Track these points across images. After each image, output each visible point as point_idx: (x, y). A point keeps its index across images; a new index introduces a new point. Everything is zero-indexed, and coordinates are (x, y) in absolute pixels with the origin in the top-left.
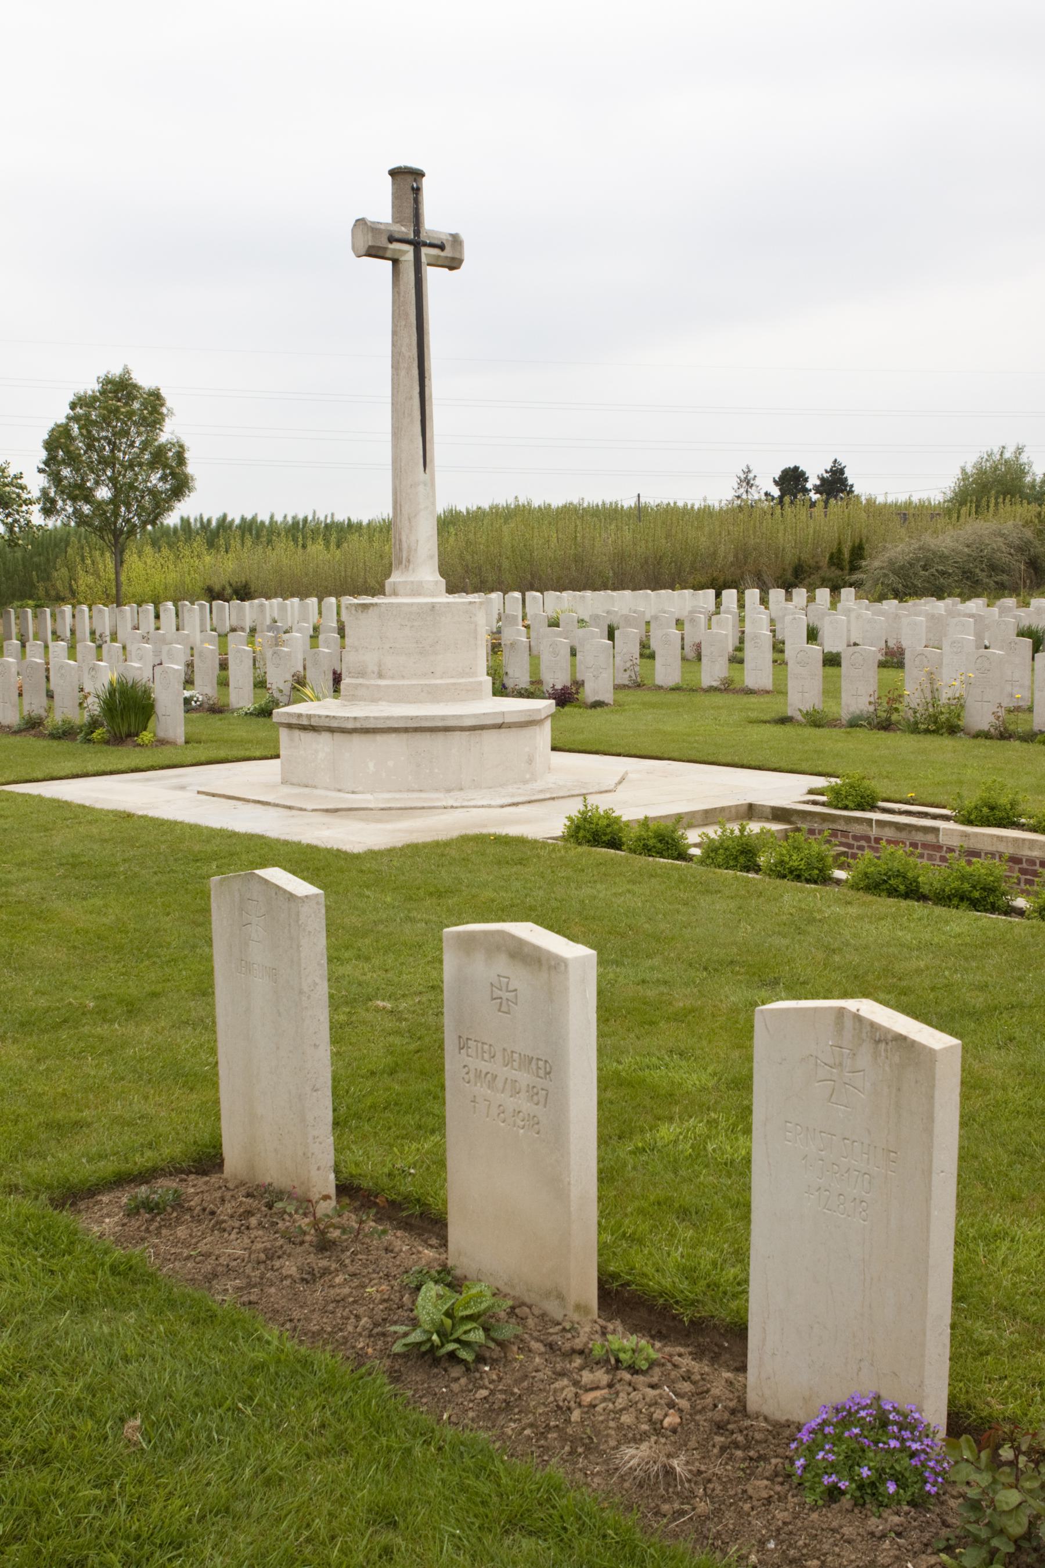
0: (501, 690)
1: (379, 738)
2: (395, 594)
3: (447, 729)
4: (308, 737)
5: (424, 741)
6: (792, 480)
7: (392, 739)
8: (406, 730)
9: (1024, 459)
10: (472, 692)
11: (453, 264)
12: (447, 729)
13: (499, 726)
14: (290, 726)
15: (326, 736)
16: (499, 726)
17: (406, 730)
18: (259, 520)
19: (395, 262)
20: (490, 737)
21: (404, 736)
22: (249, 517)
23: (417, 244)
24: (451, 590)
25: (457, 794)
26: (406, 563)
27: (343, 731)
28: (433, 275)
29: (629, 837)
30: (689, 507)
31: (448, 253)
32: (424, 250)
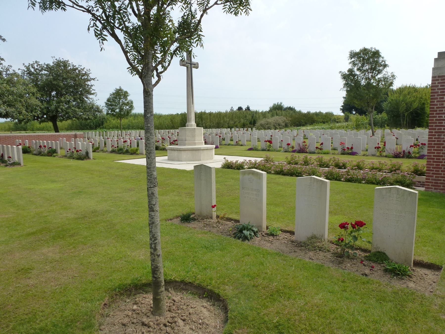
0: (206, 143)
1: (186, 152)
2: (188, 126)
3: (198, 150)
4: (173, 152)
5: (194, 152)
6: (240, 109)
7: (189, 151)
8: (191, 150)
9: (282, 105)
10: (201, 144)
11: (197, 68)
12: (198, 150)
13: (207, 149)
14: (169, 150)
15: (176, 151)
16: (207, 149)
17: (191, 150)
18: (343, 105)
19: (187, 67)
20: (205, 151)
21: (191, 151)
22: (203, 111)
23: (191, 64)
24: (197, 126)
25: (377, 165)
26: (190, 121)
27: (180, 150)
28: (194, 69)
29: (234, 166)
30: (342, 108)
31: (196, 66)
32: (192, 65)
